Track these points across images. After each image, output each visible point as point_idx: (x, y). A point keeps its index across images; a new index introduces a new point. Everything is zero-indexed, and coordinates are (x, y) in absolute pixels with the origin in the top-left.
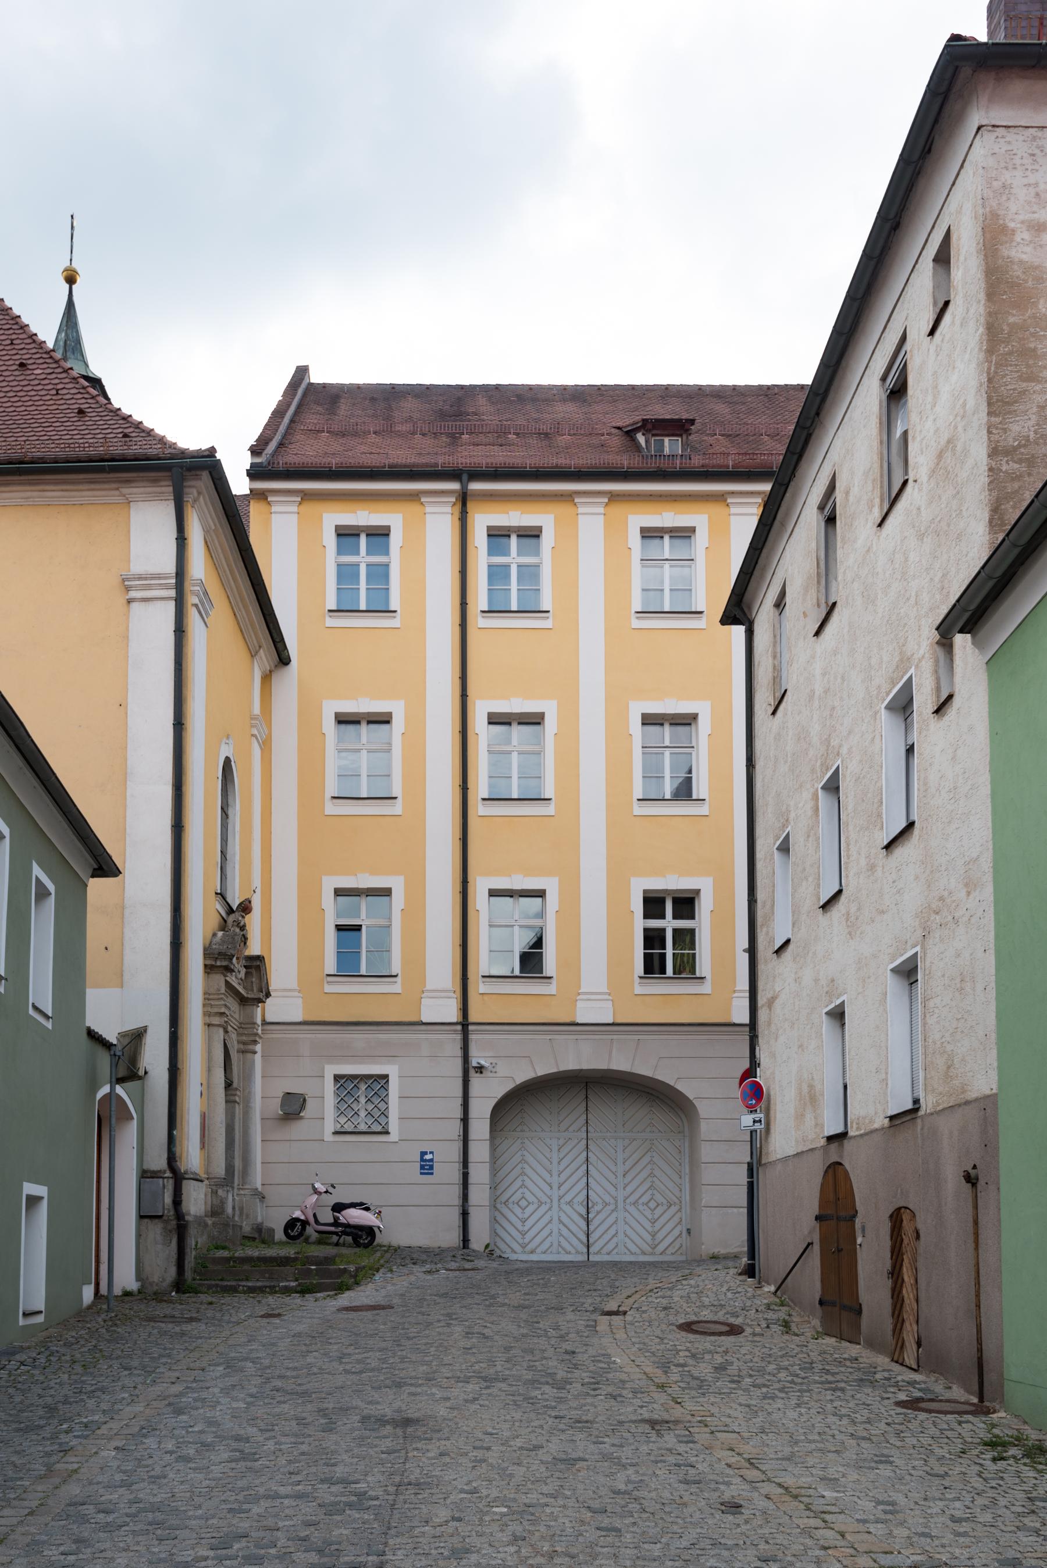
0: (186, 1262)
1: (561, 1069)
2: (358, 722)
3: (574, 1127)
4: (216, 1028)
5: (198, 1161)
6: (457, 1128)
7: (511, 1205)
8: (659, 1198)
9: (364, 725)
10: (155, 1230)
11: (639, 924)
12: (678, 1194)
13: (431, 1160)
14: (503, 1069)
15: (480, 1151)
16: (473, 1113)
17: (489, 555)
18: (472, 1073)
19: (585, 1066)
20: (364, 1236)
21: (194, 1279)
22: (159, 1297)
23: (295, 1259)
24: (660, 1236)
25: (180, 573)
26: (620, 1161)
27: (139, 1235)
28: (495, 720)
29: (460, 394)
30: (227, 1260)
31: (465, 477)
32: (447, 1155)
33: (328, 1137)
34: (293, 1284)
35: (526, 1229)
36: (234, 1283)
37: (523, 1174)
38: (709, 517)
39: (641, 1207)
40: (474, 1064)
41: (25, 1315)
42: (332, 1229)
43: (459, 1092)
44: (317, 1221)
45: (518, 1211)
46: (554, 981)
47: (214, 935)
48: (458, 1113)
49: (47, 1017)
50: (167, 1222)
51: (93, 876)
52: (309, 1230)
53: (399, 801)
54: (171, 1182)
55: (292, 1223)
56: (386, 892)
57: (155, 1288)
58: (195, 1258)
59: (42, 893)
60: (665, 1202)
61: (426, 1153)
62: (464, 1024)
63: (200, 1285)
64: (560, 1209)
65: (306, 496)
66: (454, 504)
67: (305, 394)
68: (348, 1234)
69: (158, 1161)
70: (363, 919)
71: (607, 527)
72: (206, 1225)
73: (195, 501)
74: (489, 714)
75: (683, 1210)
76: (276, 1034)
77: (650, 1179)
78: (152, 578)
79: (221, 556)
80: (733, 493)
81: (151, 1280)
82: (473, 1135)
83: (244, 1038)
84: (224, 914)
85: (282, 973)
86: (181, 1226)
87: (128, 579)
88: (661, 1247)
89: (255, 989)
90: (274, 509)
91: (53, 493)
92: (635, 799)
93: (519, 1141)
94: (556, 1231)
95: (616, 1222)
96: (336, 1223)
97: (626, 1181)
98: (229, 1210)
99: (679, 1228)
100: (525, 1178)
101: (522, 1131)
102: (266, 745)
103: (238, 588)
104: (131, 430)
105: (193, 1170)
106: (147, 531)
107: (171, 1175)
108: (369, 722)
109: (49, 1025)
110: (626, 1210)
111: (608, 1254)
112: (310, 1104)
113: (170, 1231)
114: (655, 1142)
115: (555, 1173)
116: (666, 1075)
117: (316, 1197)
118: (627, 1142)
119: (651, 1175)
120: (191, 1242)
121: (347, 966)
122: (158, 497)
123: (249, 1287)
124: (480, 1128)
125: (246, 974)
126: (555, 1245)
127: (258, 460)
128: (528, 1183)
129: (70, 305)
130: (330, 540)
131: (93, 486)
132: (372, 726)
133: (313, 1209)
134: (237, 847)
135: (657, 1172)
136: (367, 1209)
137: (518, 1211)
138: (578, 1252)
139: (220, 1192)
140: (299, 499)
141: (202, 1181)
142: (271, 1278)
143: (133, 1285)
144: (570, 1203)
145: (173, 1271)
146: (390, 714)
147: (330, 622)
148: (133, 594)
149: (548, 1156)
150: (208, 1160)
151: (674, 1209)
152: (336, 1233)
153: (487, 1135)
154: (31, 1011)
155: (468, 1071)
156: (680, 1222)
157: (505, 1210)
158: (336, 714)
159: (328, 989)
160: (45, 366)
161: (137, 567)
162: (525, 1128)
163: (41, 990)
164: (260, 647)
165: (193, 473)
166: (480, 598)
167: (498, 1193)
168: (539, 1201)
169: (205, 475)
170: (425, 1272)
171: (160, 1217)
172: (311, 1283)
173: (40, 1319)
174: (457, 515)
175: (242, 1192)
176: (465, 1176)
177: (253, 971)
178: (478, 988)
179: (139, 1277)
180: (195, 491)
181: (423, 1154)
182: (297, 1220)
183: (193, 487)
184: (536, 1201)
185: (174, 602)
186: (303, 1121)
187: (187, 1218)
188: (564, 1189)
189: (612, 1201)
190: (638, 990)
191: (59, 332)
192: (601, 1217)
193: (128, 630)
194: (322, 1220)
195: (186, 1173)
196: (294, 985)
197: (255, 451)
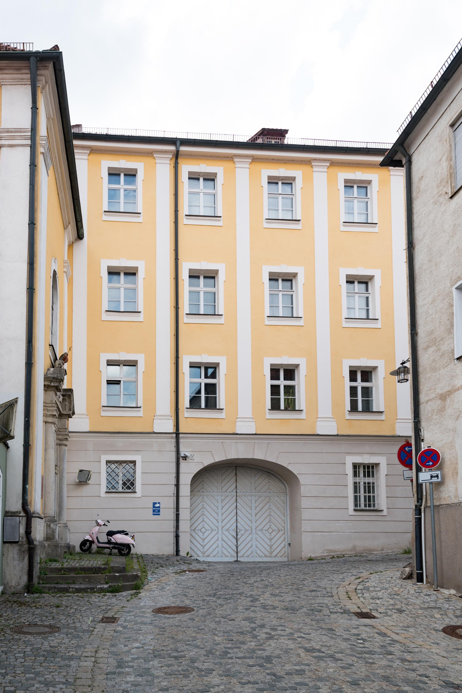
0: (34, 572)
1: (229, 458)
3: (230, 489)
4: (50, 424)
6: (172, 489)
7: (197, 531)
8: (274, 527)
11: (269, 382)
12: (283, 525)
13: (159, 507)
15: (185, 502)
18: (181, 459)
19: (241, 457)
21: (39, 583)
23: (105, 569)
24: (274, 547)
26: (253, 508)
30: (59, 570)
32: (167, 505)
33: (103, 494)
34: (106, 586)
35: (205, 544)
36: (66, 586)
37: (203, 514)
38: (303, 173)
39: (264, 532)
40: (182, 455)
42: (107, 545)
43: (174, 470)
45: (201, 534)
46: (224, 411)
47: (48, 369)
48: (174, 481)
50: (21, 546)
52: (94, 547)
55: (84, 542)
57: (13, 590)
60: (277, 529)
61: (156, 503)
64: (223, 533)
71: (251, 174)
72: (45, 547)
73: (43, 88)
75: (286, 533)
77: (269, 517)
78: (16, 132)
80: (315, 160)
81: (10, 584)
83: (61, 437)
85: (80, 402)
86: (30, 548)
88: (275, 553)
89: (67, 409)
92: (266, 316)
93: (201, 497)
94: (220, 545)
95: (251, 540)
96: (109, 542)
97: (257, 518)
98: (57, 537)
99: (284, 543)
100: (204, 517)
101: (203, 492)
105: (38, 511)
107: (24, 515)
110: (257, 534)
111: (247, 557)
114: (271, 498)
115: (220, 514)
116: (282, 461)
117: (98, 527)
118: (257, 498)
119: (270, 515)
120: (37, 559)
122: (20, 82)
123: (76, 589)
124: (185, 490)
125: (63, 399)
126: (220, 552)
128: (206, 519)
133: (97, 534)
134: (58, 328)
135: (272, 513)
136: (127, 534)
137: (201, 534)
138: (232, 556)
139: (52, 525)
140: (89, 152)
141: (42, 518)
142: (89, 582)
144: (227, 530)
145: (25, 579)
147: (105, 218)
149: (217, 505)
150: (44, 505)
151: (281, 533)
153: (188, 493)
155: (179, 458)
156: (284, 540)
158: (108, 266)
159: (103, 414)
162: (204, 490)
164: (69, 223)
168: (212, 529)
169: (51, 66)
170: (176, 573)
174: (173, 164)
176: (177, 515)
177: (67, 398)
181: (154, 504)
182: (87, 540)
184: (210, 529)
186: (88, 486)
187: (35, 543)
188: (225, 522)
189: (250, 529)
190: (268, 416)
192: (244, 537)
194: (101, 541)
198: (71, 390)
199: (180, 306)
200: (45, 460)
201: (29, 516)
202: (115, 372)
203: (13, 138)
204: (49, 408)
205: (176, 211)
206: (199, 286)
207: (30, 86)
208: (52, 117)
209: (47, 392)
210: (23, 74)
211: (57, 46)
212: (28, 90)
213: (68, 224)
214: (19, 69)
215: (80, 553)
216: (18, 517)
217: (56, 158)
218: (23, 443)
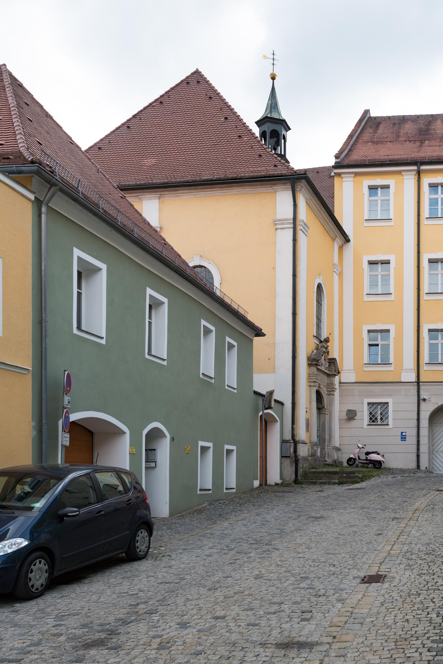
2: (378, 264)
5: (305, 436)
6: (415, 422)
7: (439, 453)
9: (380, 265)
10: (287, 462)
13: (405, 435)
14: (433, 400)
15: (424, 432)
16: (422, 417)
17: (430, 194)
18: (421, 401)
20: (378, 465)
22: (288, 485)
23: (339, 472)
25: (295, 219)
27: (281, 464)
28: (431, 261)
29: (430, 119)
31: (419, 164)
32: (411, 433)
33: (365, 426)
36: (315, 481)
40: (422, 398)
41: (226, 489)
42: (365, 462)
43: (416, 409)
44: (359, 459)
47: (313, 352)
48: (416, 417)
49: (235, 389)
50: (291, 459)
51: (256, 336)
52: (357, 462)
53: (393, 295)
54: (293, 444)
55: (350, 459)
56: (388, 331)
57: (288, 482)
58: (302, 472)
59: (231, 347)
61: (403, 433)
62: (418, 382)
65: (356, 174)
66: (415, 175)
67: (368, 120)
69: (288, 436)
70: (379, 342)
72: (308, 460)
74: (429, 259)
76: (345, 387)
78: (284, 220)
82: (422, 425)
84: (318, 343)
86: (296, 461)
87: (276, 221)
89: (333, 371)
90: (344, 180)
91: (248, 189)
96: (367, 460)
102: (341, 275)
103: (323, 217)
104: (278, 162)
105: (302, 440)
108: (382, 263)
109: (236, 391)
112: (358, 414)
117: (359, 449)
120: (300, 466)
123: (321, 482)
127: (338, 160)
129: (273, 88)
130: (366, 191)
131: (262, 186)
132: (383, 265)
133: (358, 454)
136: (379, 454)
139: (314, 448)
141: (306, 444)
143: (279, 481)
145: (294, 477)
146: (389, 260)
147: (366, 224)
152: (367, 463)
154: (226, 387)
157: (436, 454)
159: (365, 369)
160: (248, 136)
161: (279, 217)
163: (231, 378)
166: (426, 212)
167: (434, 447)
171: (289, 457)
173: (234, 491)
174: (416, 179)
176: (418, 441)
177: (332, 364)
178: (424, 368)
179: (281, 478)
180: (300, 187)
181: (402, 433)
186: (355, 421)
187: (298, 457)
191: (269, 101)
193: (276, 240)
194: (361, 458)
195: (299, 441)
196: (352, 368)
197: (337, 157)
199: (421, 288)
201: (296, 443)
204: (311, 377)
205: (419, 215)
206: (437, 270)
212: (290, 193)
215: (347, 467)
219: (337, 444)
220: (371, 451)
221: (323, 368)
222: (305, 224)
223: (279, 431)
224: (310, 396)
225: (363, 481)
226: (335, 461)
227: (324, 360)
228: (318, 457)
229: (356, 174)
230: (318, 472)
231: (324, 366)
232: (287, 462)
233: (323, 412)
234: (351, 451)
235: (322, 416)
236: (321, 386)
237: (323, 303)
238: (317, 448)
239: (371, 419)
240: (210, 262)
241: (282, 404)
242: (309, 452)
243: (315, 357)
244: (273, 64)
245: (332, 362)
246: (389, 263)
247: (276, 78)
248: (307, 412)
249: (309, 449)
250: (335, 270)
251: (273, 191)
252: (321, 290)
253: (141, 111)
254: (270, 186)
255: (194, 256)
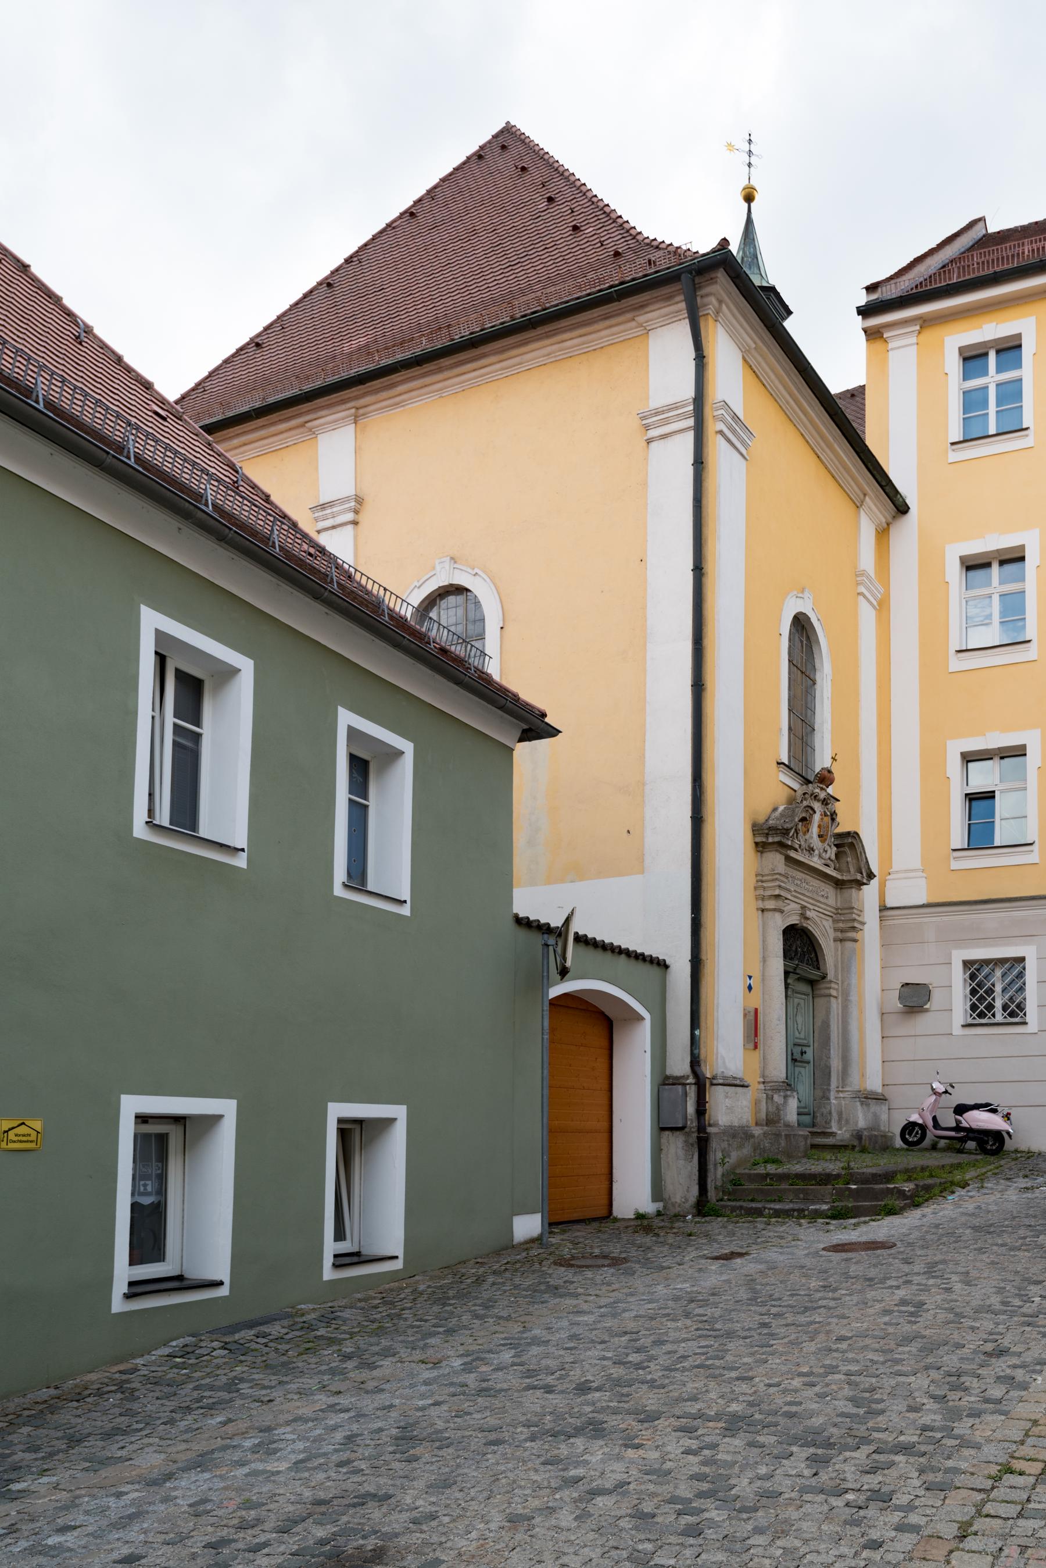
0: (709, 1180)
2: (988, 565)
4: (771, 913)
20: (991, 1143)
33: (957, 1030)
34: (825, 1207)
42: (952, 1134)
50: (688, 1134)
51: (520, 740)
53: (1033, 645)
54: (694, 1088)
56: (1019, 752)
57: (678, 1209)
58: (723, 1175)
63: (725, 1207)
68: (972, 1139)
69: (679, 1065)
73: (718, 312)
76: (898, 920)
78: (669, 410)
79: (777, 382)
81: (673, 1200)
83: (841, 925)
86: (702, 1144)
89: (852, 870)
90: (891, 345)
96: (958, 1128)
102: (882, 607)
103: (811, 422)
106: (662, 355)
108: (1002, 563)
112: (937, 996)
113: (692, 1145)
117: (934, 1097)
120: (715, 1154)
121: (980, 836)
123: (776, 1210)
129: (749, 222)
130: (953, 364)
131: (608, 323)
132: (1008, 568)
133: (931, 1111)
136: (994, 1111)
139: (776, 1098)
140: (918, 327)
143: (649, 1207)
145: (695, 1190)
147: (954, 456)
148: (653, 433)
158: (961, 558)
159: (955, 865)
164: (865, 495)
165: (707, 276)
169: (721, 275)
172: (847, 1207)
175: (841, 1095)
177: (847, 849)
180: (713, 300)
182: (913, 1124)
183: (707, 295)
185: (692, 432)
186: (928, 1014)
195: (714, 1078)
196: (917, 864)
198: (855, 835)
200: (763, 980)
202: (982, 777)
203: (666, 422)
204: (765, 885)
207: (687, 321)
208: (753, 346)
209: (765, 855)
210: (677, 303)
211: (725, 239)
212: (683, 329)
213: (862, 496)
214: (669, 298)
215: (902, 1149)
216: (680, 1087)
217: (788, 403)
218: (689, 958)
219: (874, 1083)
220: (971, 1102)
221: (816, 862)
222: (735, 417)
223: (648, 1047)
224: (764, 941)
225: (917, 1205)
226: (858, 1136)
227: (820, 836)
228: (787, 1125)
229: (926, 322)
230: (775, 1175)
231: (820, 856)
232: (675, 1144)
233: (823, 992)
234: (915, 1106)
235: (820, 1002)
236: (809, 914)
237: (818, 677)
238: (786, 1097)
239: (974, 1007)
240: (476, 570)
241: (662, 965)
242: (757, 1112)
243: (779, 824)
244: (750, 165)
245: (848, 844)
246: (1022, 559)
247: (757, 197)
248: (750, 988)
249: (757, 1102)
250: (862, 589)
251: (639, 331)
252: (812, 638)
253: (366, 245)
254: (629, 316)
255: (437, 562)
